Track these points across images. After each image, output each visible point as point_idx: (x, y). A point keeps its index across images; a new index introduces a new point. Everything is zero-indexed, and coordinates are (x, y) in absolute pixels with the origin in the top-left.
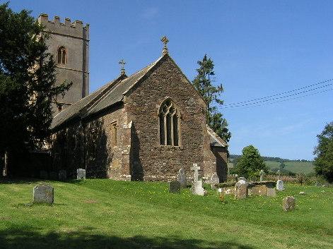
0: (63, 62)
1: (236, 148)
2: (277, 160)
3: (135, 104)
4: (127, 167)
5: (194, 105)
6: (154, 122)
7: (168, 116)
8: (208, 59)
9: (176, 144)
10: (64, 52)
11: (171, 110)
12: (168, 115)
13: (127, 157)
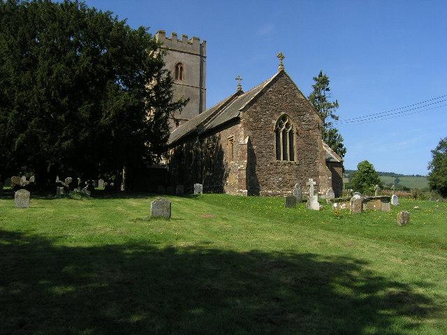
0: (181, 78)
3: (251, 120)
4: (244, 182)
6: (271, 138)
7: (284, 132)
8: (323, 75)
9: (292, 159)
10: (182, 68)
11: (287, 126)
13: (244, 173)
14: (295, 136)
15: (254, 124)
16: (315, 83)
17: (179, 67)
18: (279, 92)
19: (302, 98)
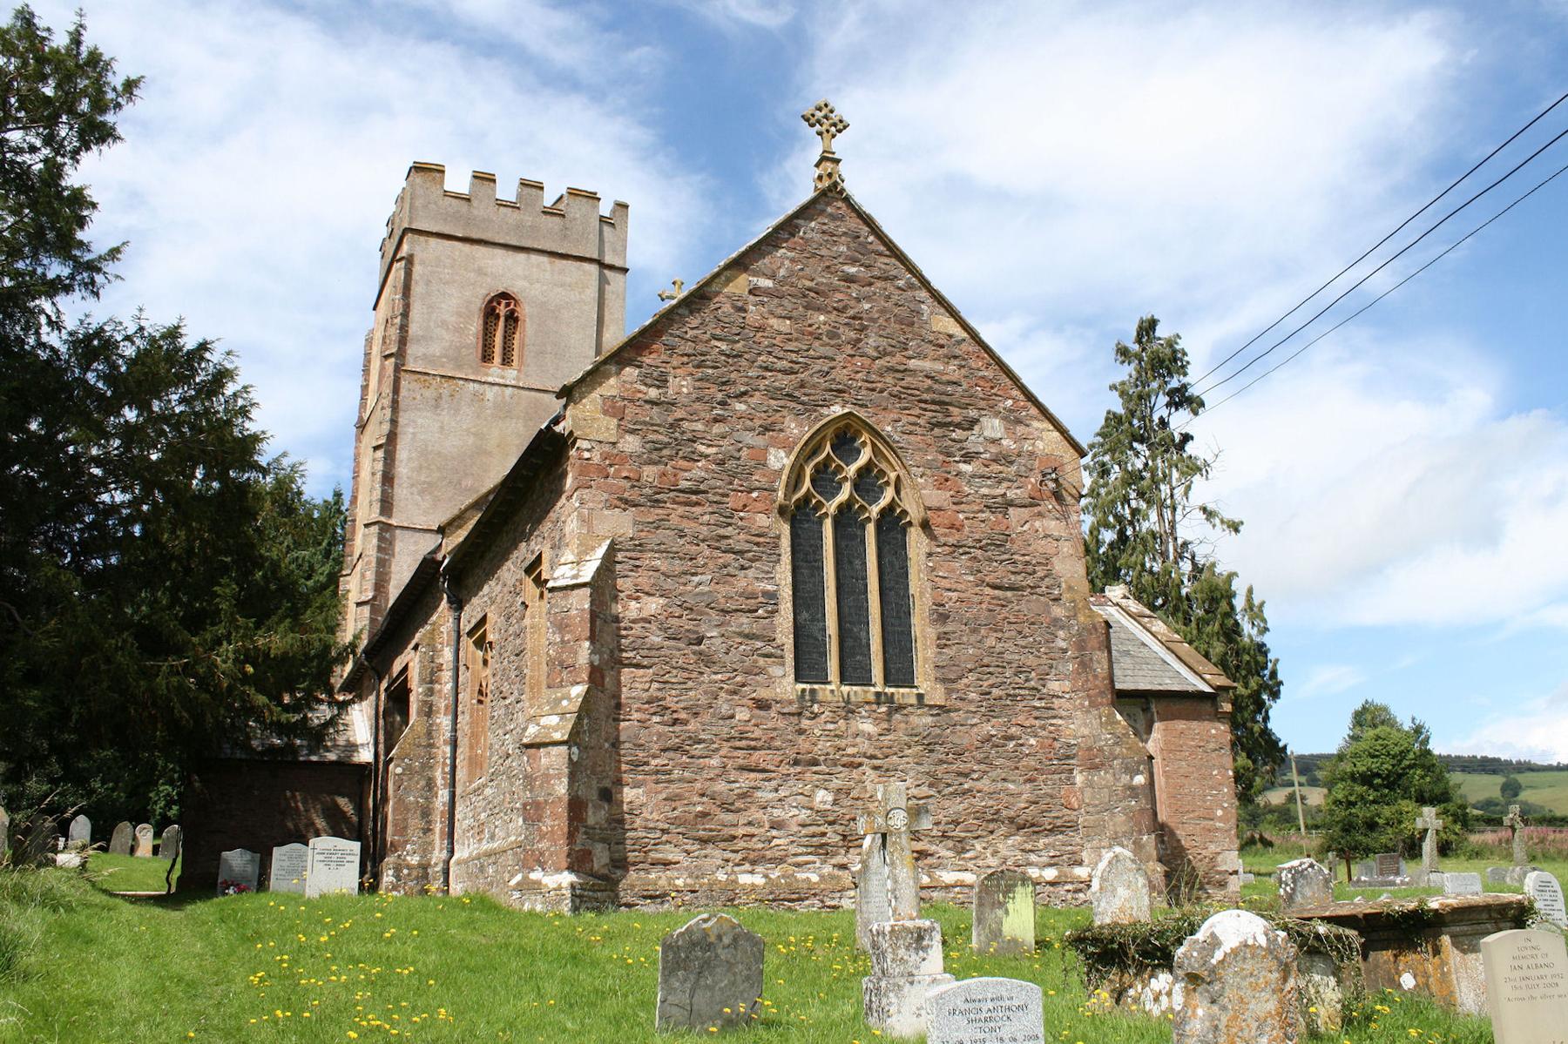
0: (507, 360)
1: (1308, 722)
2: (1488, 766)
4: (555, 822)
5: (1004, 459)
6: (765, 545)
7: (847, 520)
8: (1162, 332)
9: (900, 671)
10: (512, 319)
11: (867, 482)
12: (845, 509)
13: (555, 760)
14: (917, 543)
15: (650, 473)
17: (502, 310)
18: (813, 298)
19: (959, 333)
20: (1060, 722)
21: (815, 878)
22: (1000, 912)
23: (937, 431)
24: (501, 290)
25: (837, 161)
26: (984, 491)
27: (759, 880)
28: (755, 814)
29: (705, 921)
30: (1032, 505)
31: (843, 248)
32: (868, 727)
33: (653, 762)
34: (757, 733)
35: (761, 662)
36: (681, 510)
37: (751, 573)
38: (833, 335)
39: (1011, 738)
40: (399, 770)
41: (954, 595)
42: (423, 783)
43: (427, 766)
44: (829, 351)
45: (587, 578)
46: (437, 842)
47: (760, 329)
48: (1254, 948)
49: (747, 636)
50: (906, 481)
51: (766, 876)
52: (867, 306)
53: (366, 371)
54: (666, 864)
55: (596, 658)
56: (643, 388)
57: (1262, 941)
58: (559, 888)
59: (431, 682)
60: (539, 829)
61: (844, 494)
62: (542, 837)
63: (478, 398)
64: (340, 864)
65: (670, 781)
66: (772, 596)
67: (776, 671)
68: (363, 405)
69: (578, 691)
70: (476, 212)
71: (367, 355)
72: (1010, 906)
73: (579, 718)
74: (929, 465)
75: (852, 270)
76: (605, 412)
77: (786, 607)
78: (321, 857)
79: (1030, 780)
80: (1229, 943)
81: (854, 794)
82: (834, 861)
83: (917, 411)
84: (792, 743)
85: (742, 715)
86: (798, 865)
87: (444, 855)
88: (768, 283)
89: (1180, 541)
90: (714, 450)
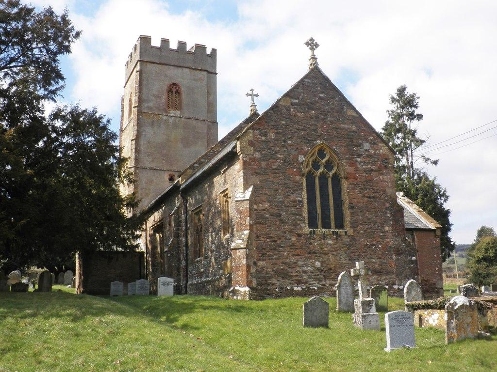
3: (257, 155)
5: (370, 156)
9: (340, 225)
11: (329, 165)
12: (322, 174)
14: (345, 184)
15: (263, 164)
16: (393, 107)
17: (174, 90)
20: (388, 240)
21: (316, 288)
22: (378, 298)
23: (349, 147)
24: (173, 82)
25: (316, 58)
26: (364, 167)
27: (300, 289)
28: (297, 269)
29: (314, 298)
30: (379, 171)
31: (319, 88)
32: (330, 242)
33: (268, 253)
34: (298, 244)
35: (298, 222)
36: (273, 175)
37: (294, 195)
38: (317, 117)
39: (373, 245)
40: (169, 255)
41: (356, 200)
42: (177, 259)
43: (178, 254)
44: (316, 123)
45: (248, 198)
46: (182, 278)
47: (295, 116)
48: (466, 305)
49: (294, 214)
50: (340, 165)
51: (302, 288)
52: (327, 107)
53: (122, 111)
54: (273, 284)
55: (251, 222)
56: (260, 137)
57: (468, 304)
58: (245, 291)
59: (178, 226)
60: (238, 274)
61: (321, 170)
62: (239, 276)
63: (167, 122)
64: (168, 285)
65: (273, 259)
66: (301, 202)
67: (303, 225)
68: (122, 123)
69: (247, 232)
70: (163, 54)
71: (123, 105)
72: (381, 296)
73: (248, 241)
74: (346, 159)
75: (322, 95)
76: (249, 145)
77: (305, 205)
78: (162, 284)
79: (380, 258)
80: (459, 304)
81: (326, 262)
82: (321, 283)
83: (343, 142)
84: (308, 247)
85: (294, 239)
86: (310, 284)
87: (185, 282)
88: (297, 101)
89: (414, 169)
90: (282, 156)
